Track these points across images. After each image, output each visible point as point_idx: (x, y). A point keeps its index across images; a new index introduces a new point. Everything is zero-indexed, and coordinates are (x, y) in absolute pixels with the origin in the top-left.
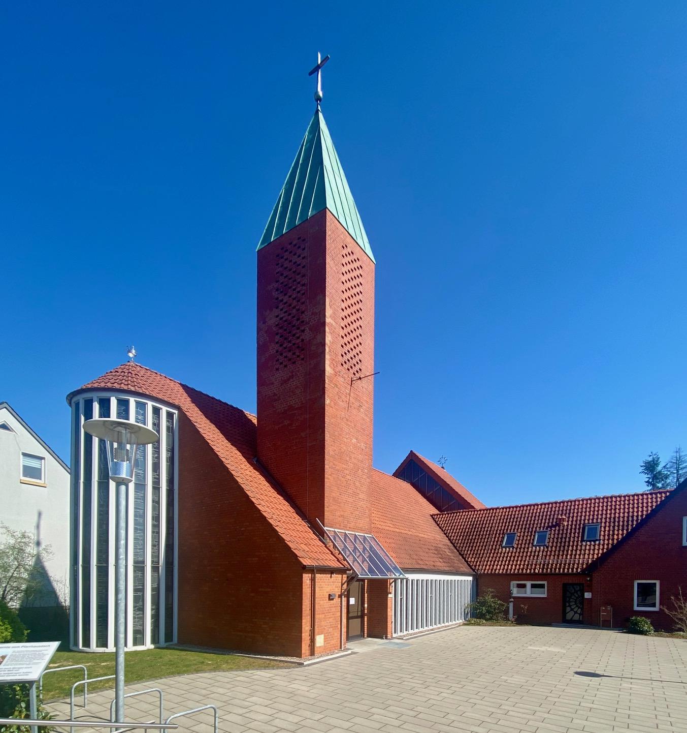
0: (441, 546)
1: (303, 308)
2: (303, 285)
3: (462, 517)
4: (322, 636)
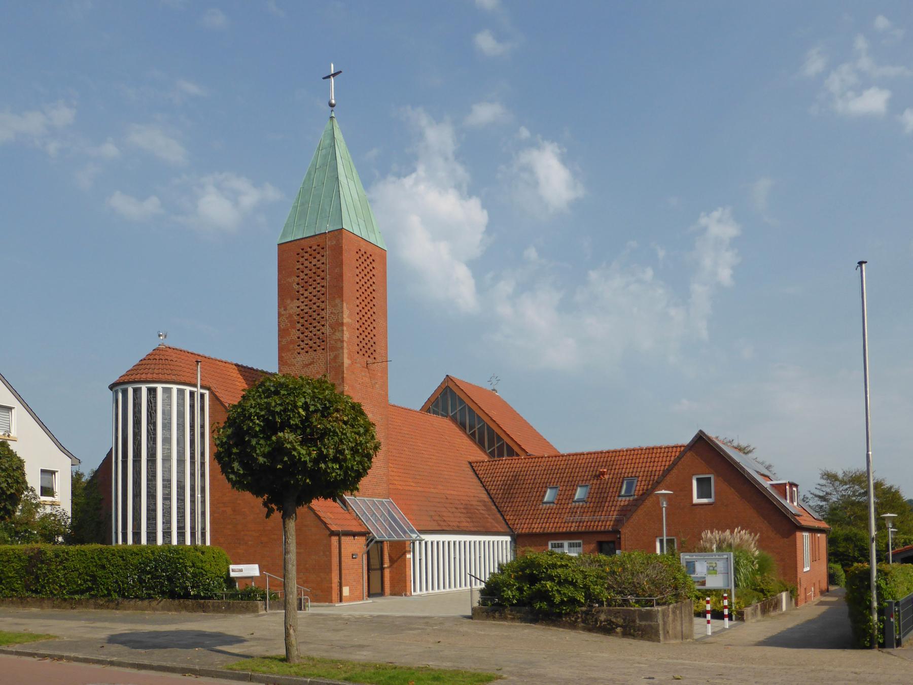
0: (474, 503)
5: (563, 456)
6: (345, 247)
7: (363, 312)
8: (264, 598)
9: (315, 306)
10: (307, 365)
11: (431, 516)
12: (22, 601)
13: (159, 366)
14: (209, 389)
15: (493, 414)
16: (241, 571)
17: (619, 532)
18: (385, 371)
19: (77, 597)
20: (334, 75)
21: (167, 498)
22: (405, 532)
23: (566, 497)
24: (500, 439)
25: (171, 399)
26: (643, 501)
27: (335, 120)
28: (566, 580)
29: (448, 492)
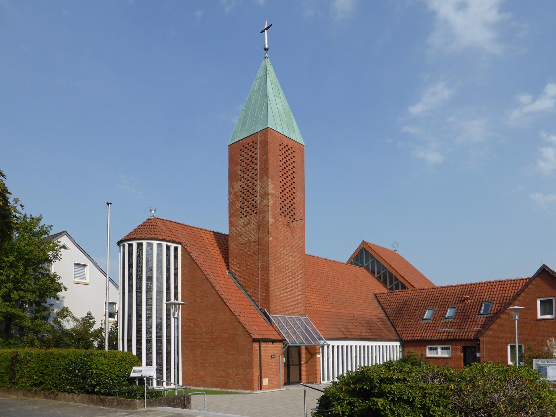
1: (255, 183)
2: (256, 170)
3: (399, 294)
4: (267, 379)
5: (438, 288)
6: (270, 140)
7: (285, 187)
8: (143, 397)
9: (251, 184)
10: (246, 225)
11: (339, 328)
13: (150, 229)
14: (180, 244)
15: (393, 264)
17: (479, 340)
18: (303, 228)
20: (267, 29)
21: (149, 317)
22: (314, 340)
23: (439, 315)
24: (396, 279)
26: (498, 317)
27: (268, 59)
28: (400, 399)
29: (356, 313)
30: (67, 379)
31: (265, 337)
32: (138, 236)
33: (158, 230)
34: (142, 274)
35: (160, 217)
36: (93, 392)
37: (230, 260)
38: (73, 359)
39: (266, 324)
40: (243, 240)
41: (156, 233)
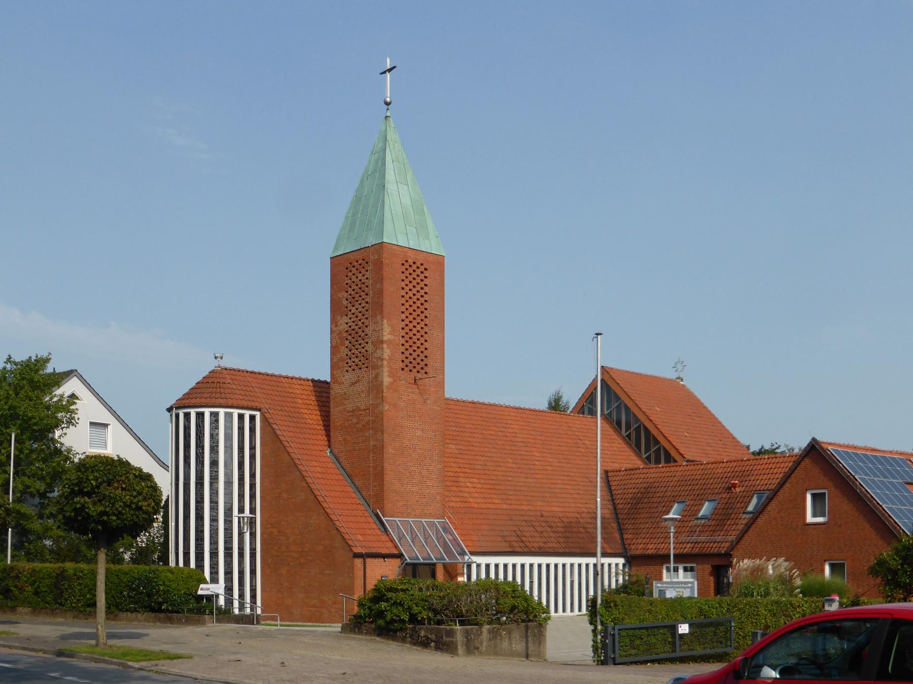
3: (659, 471)
6: (386, 261)
8: (212, 613)
9: (360, 323)
10: (353, 384)
11: (503, 537)
12: (53, 613)
13: (215, 388)
14: (259, 410)
16: (208, 589)
19: (88, 609)
20: (390, 70)
21: (214, 520)
23: (690, 513)
24: (657, 442)
25: (226, 421)
27: (391, 121)
30: (130, 597)
31: (373, 551)
32: (198, 401)
33: (226, 391)
34: (203, 458)
35: (228, 366)
36: (160, 610)
37: (332, 434)
38: (136, 576)
39: (379, 532)
40: (350, 407)
41: (223, 395)
